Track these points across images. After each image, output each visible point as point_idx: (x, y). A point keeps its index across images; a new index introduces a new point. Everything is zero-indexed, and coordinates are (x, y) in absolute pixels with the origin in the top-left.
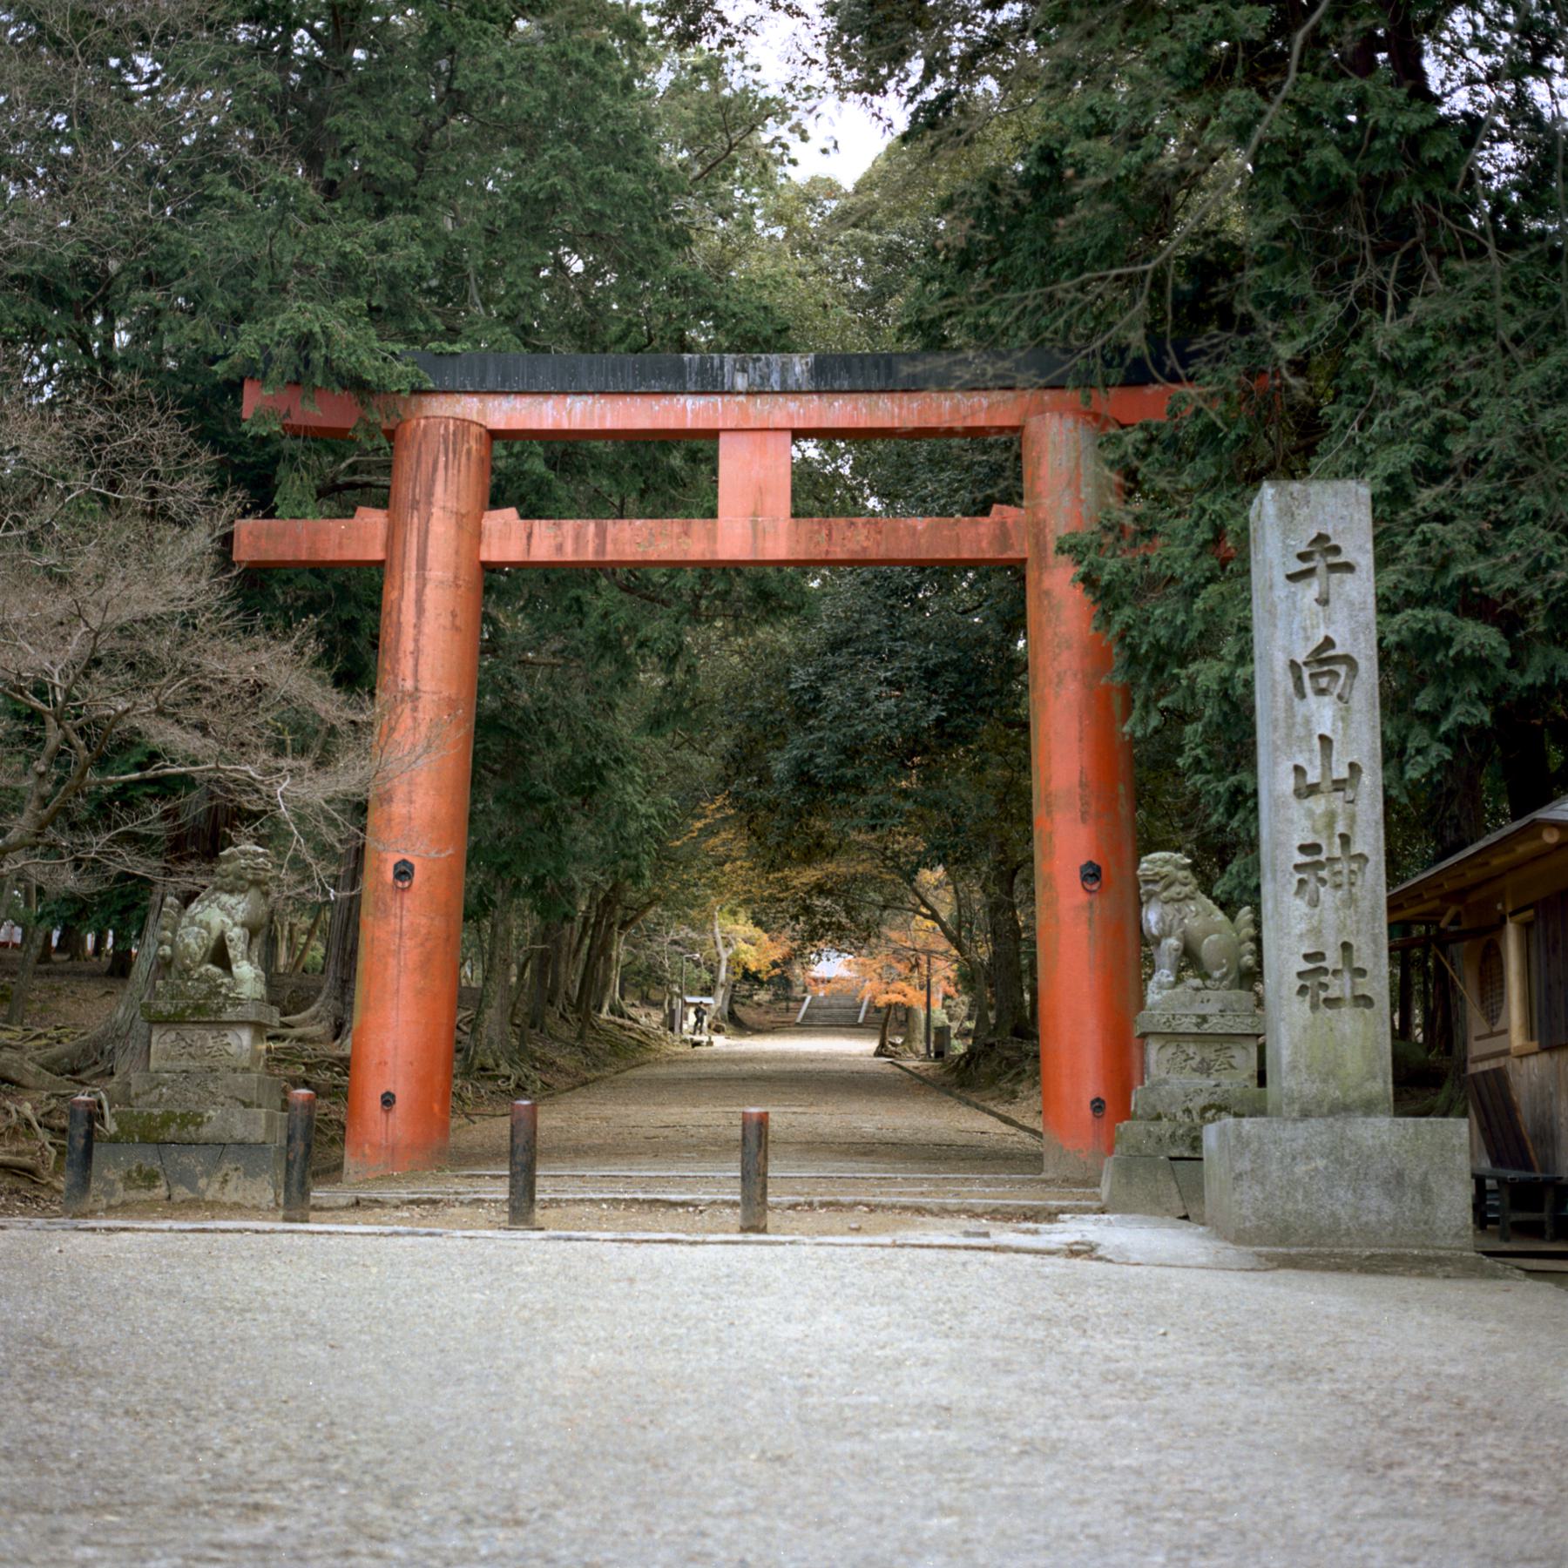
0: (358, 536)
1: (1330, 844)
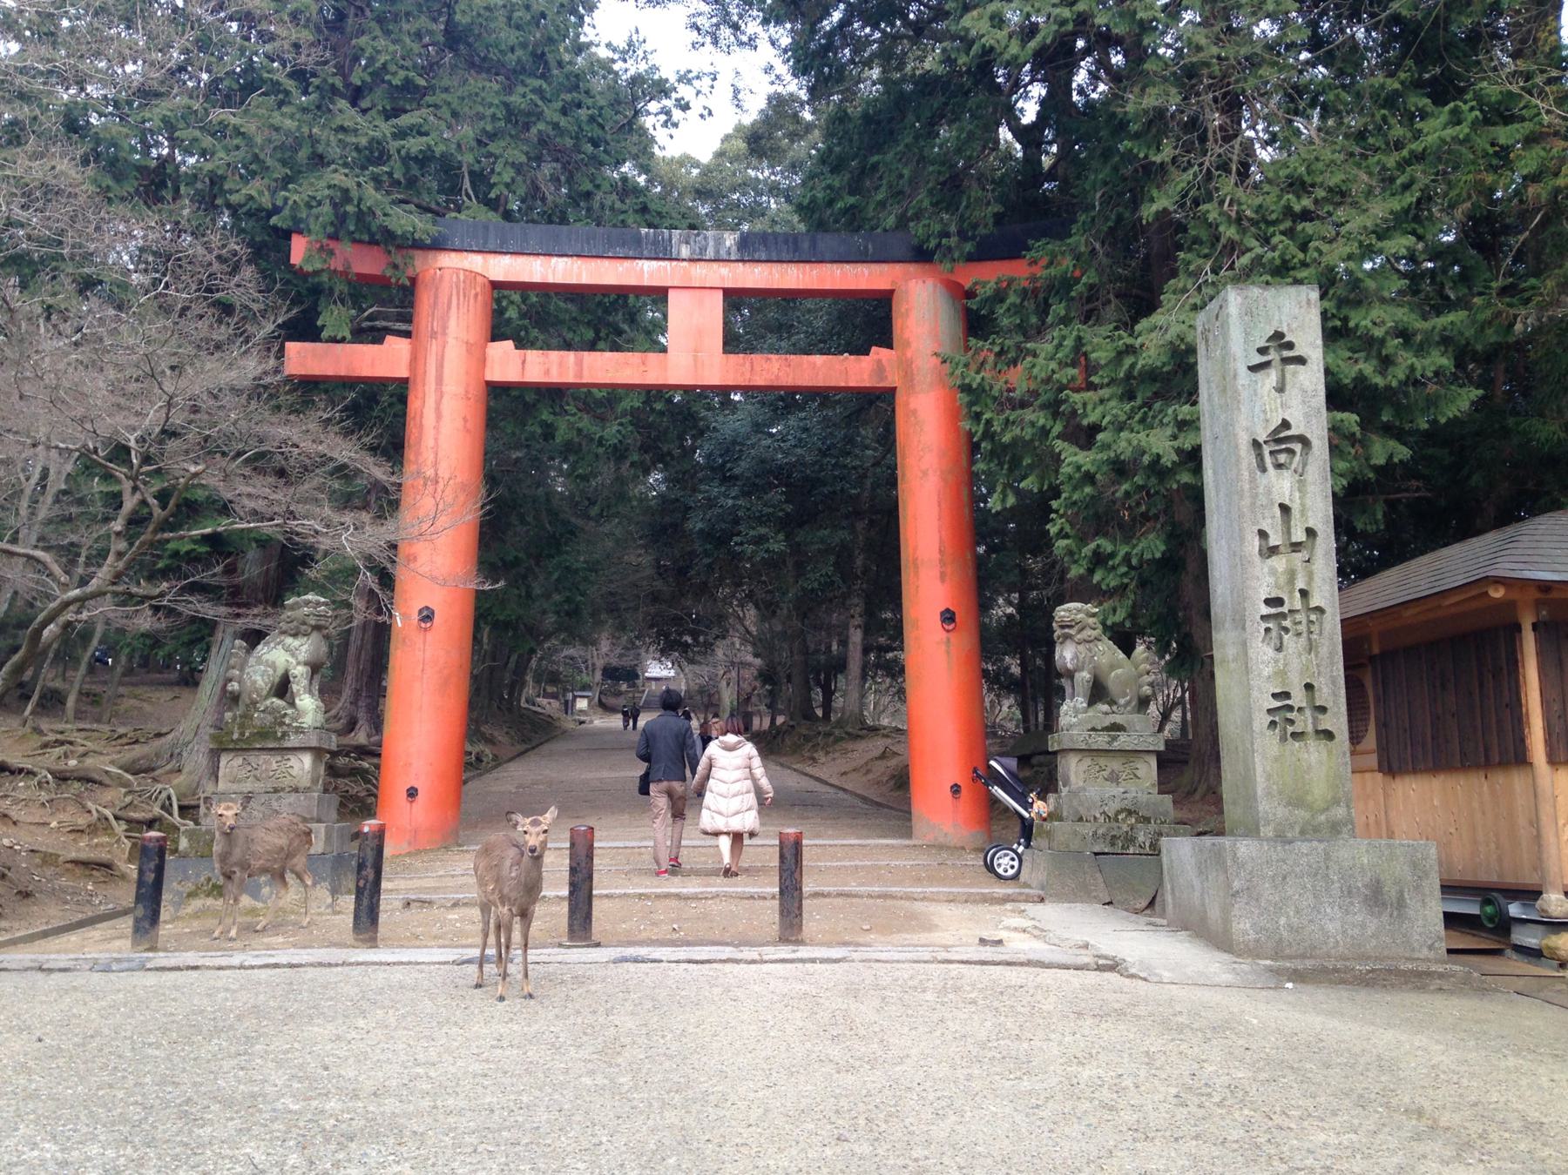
0: (384, 359)
1: (1291, 597)
